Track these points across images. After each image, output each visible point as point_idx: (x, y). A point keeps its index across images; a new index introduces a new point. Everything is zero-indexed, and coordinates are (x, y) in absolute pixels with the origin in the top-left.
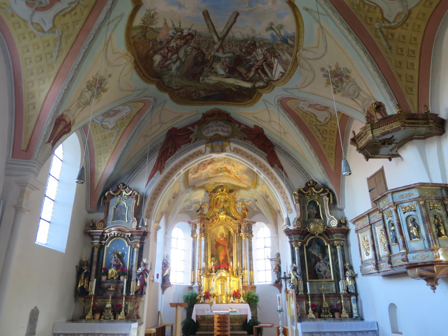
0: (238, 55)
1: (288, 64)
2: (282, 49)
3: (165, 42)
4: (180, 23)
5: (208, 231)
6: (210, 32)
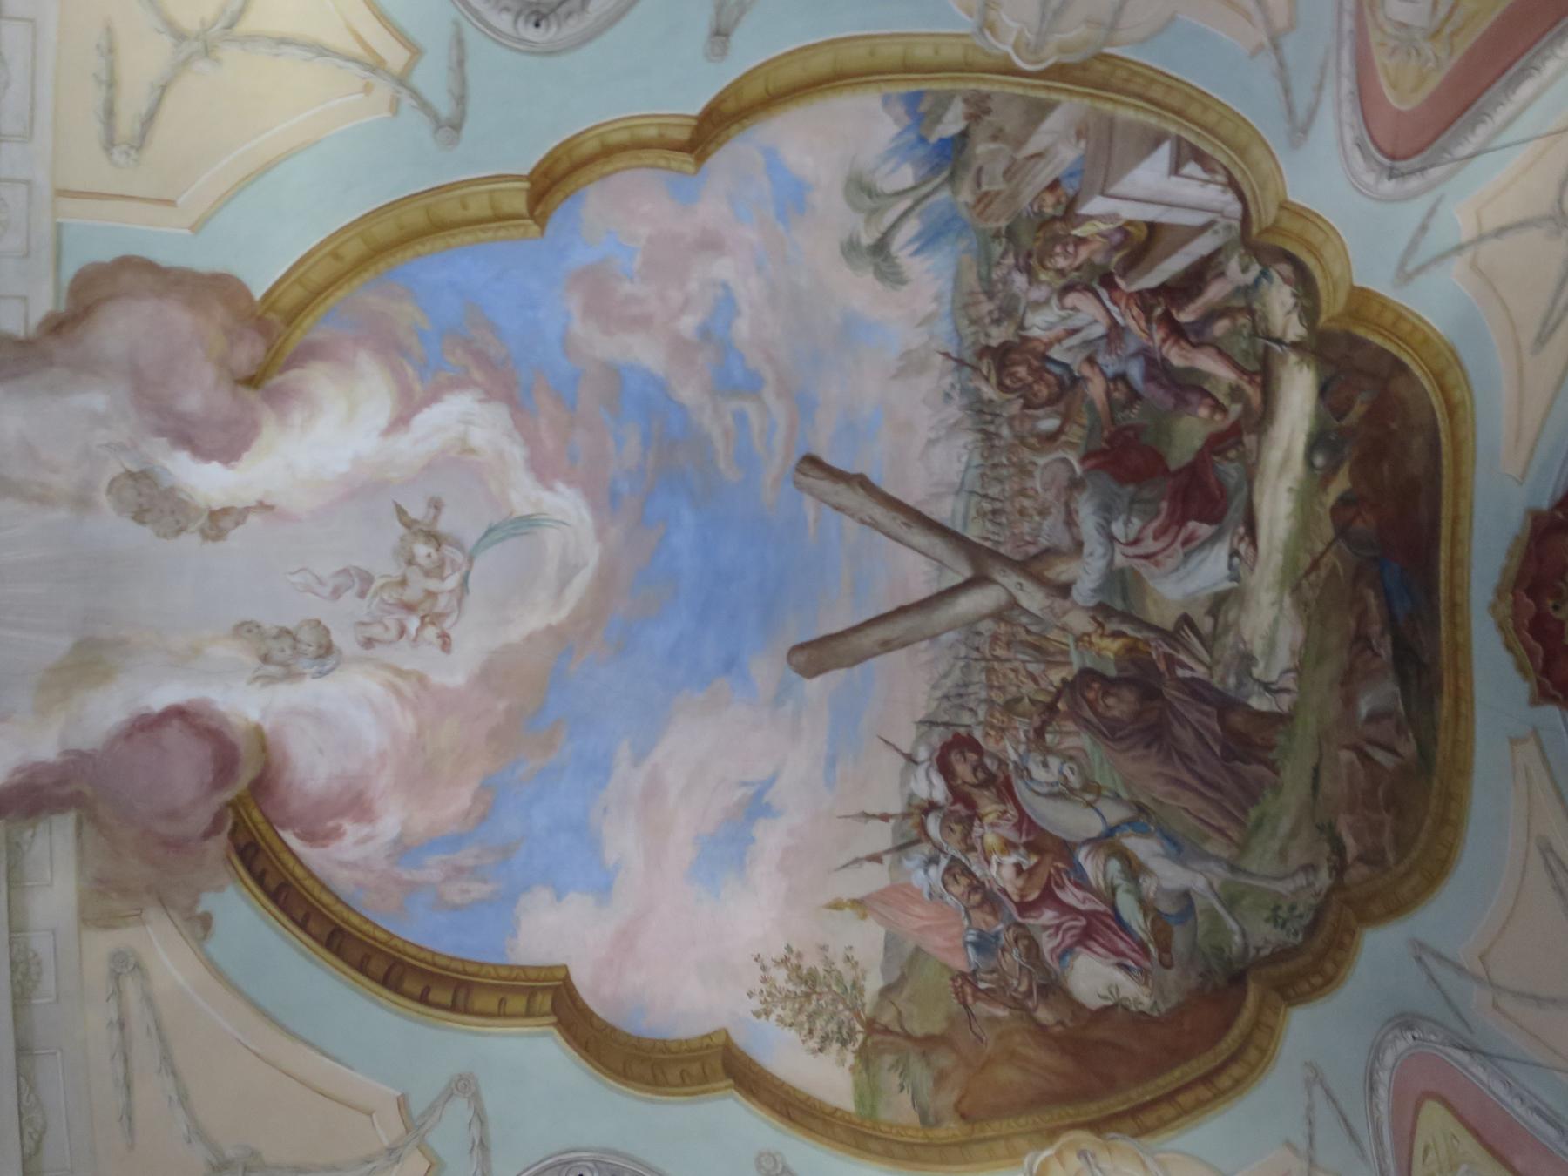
0: (1083, 460)
1: (1111, 123)
2: (1008, 174)
3: (983, 919)
4: (867, 816)
6: (933, 637)
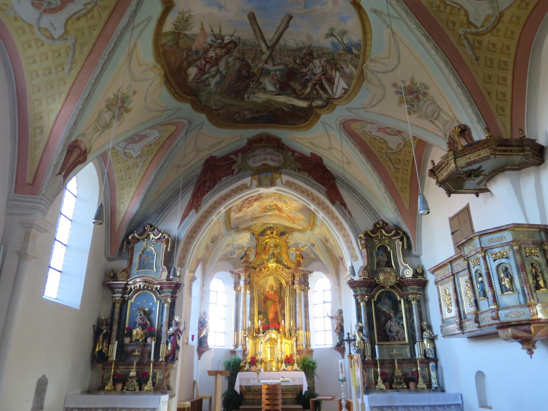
0: (291, 67)
1: (352, 79)
2: (344, 60)
3: (202, 51)
4: (220, 28)
5: (255, 283)
6: (257, 39)
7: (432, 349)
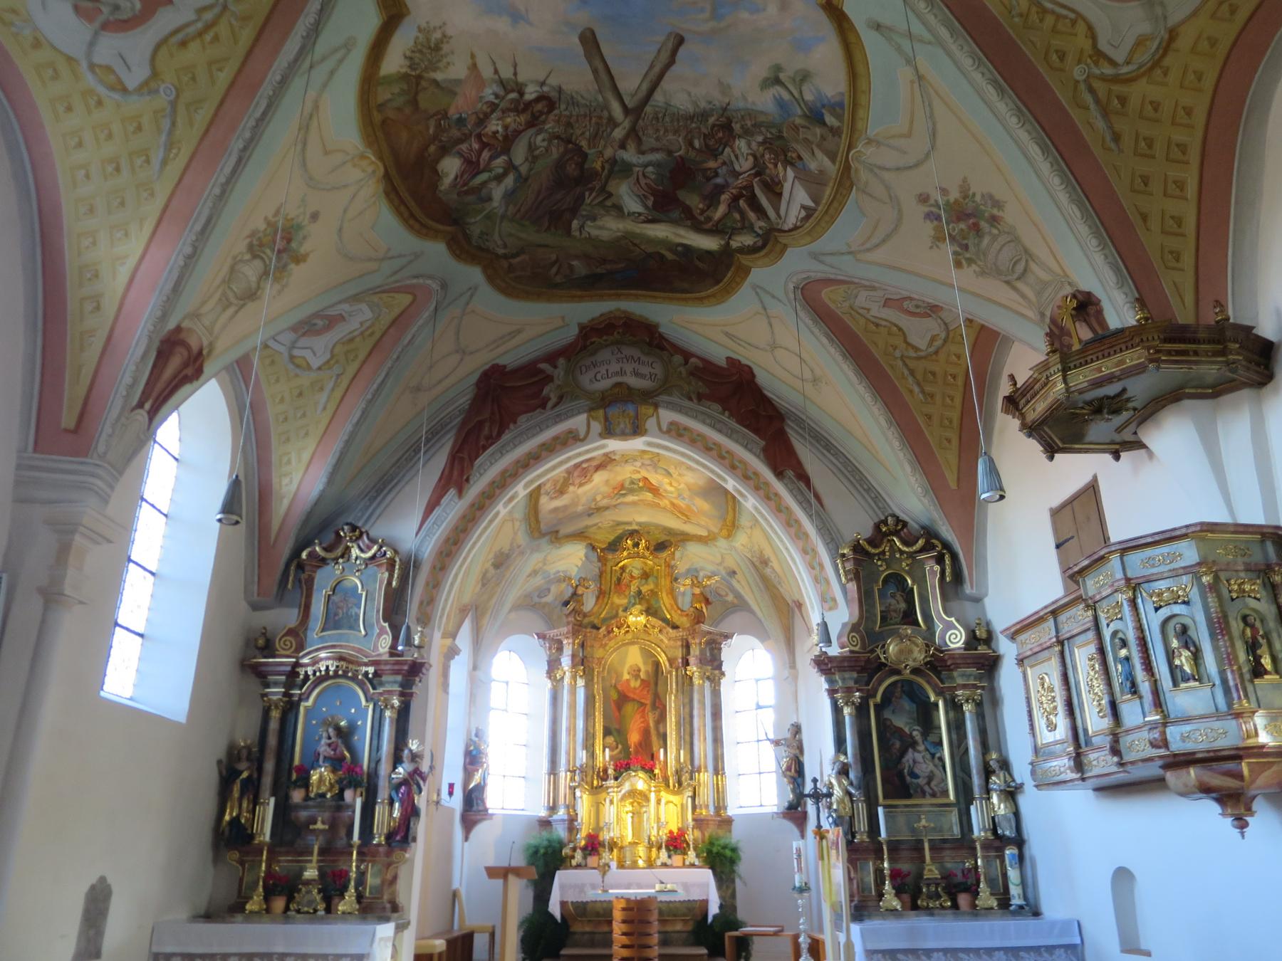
0: (680, 156)
1: (823, 184)
2: (806, 140)
3: (472, 120)
4: (515, 66)
5: (596, 661)
6: (600, 91)
7: (1011, 816)
